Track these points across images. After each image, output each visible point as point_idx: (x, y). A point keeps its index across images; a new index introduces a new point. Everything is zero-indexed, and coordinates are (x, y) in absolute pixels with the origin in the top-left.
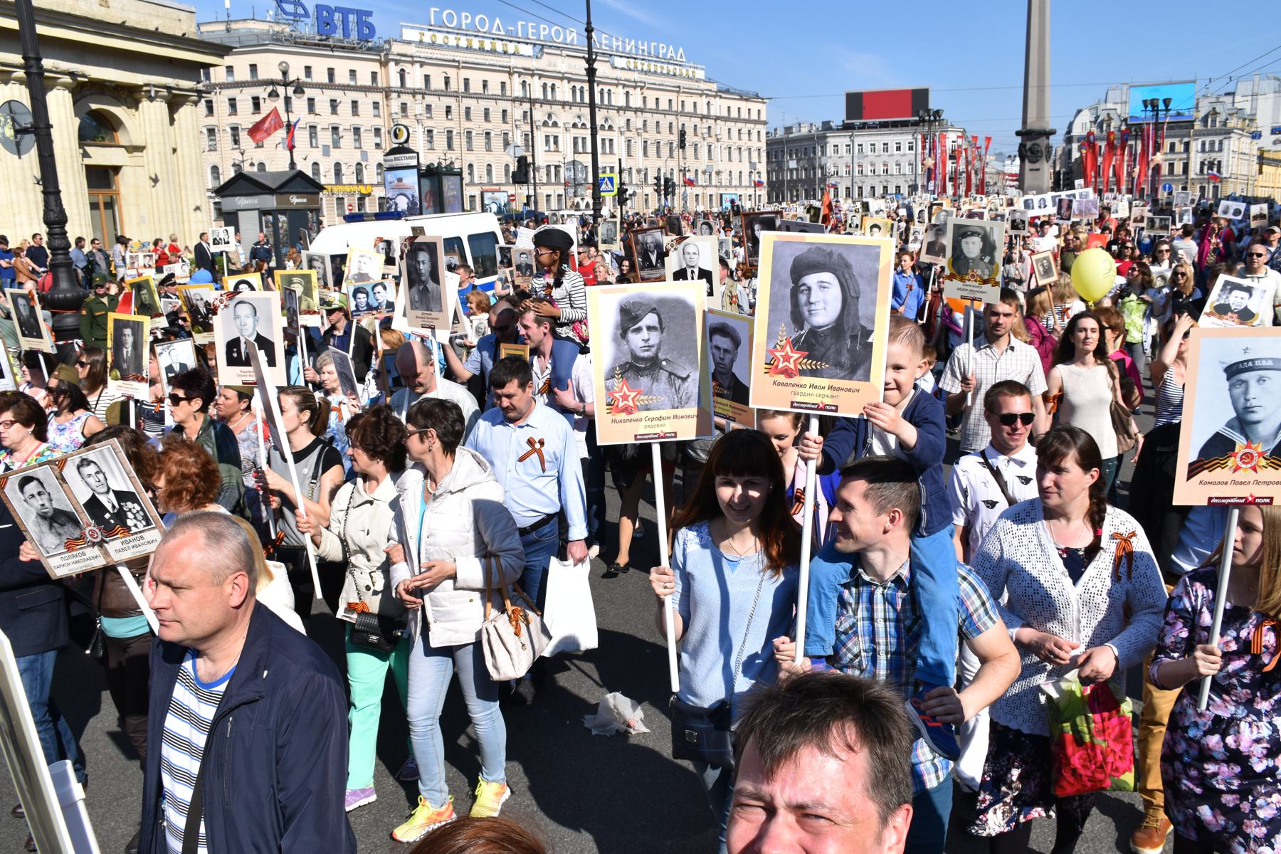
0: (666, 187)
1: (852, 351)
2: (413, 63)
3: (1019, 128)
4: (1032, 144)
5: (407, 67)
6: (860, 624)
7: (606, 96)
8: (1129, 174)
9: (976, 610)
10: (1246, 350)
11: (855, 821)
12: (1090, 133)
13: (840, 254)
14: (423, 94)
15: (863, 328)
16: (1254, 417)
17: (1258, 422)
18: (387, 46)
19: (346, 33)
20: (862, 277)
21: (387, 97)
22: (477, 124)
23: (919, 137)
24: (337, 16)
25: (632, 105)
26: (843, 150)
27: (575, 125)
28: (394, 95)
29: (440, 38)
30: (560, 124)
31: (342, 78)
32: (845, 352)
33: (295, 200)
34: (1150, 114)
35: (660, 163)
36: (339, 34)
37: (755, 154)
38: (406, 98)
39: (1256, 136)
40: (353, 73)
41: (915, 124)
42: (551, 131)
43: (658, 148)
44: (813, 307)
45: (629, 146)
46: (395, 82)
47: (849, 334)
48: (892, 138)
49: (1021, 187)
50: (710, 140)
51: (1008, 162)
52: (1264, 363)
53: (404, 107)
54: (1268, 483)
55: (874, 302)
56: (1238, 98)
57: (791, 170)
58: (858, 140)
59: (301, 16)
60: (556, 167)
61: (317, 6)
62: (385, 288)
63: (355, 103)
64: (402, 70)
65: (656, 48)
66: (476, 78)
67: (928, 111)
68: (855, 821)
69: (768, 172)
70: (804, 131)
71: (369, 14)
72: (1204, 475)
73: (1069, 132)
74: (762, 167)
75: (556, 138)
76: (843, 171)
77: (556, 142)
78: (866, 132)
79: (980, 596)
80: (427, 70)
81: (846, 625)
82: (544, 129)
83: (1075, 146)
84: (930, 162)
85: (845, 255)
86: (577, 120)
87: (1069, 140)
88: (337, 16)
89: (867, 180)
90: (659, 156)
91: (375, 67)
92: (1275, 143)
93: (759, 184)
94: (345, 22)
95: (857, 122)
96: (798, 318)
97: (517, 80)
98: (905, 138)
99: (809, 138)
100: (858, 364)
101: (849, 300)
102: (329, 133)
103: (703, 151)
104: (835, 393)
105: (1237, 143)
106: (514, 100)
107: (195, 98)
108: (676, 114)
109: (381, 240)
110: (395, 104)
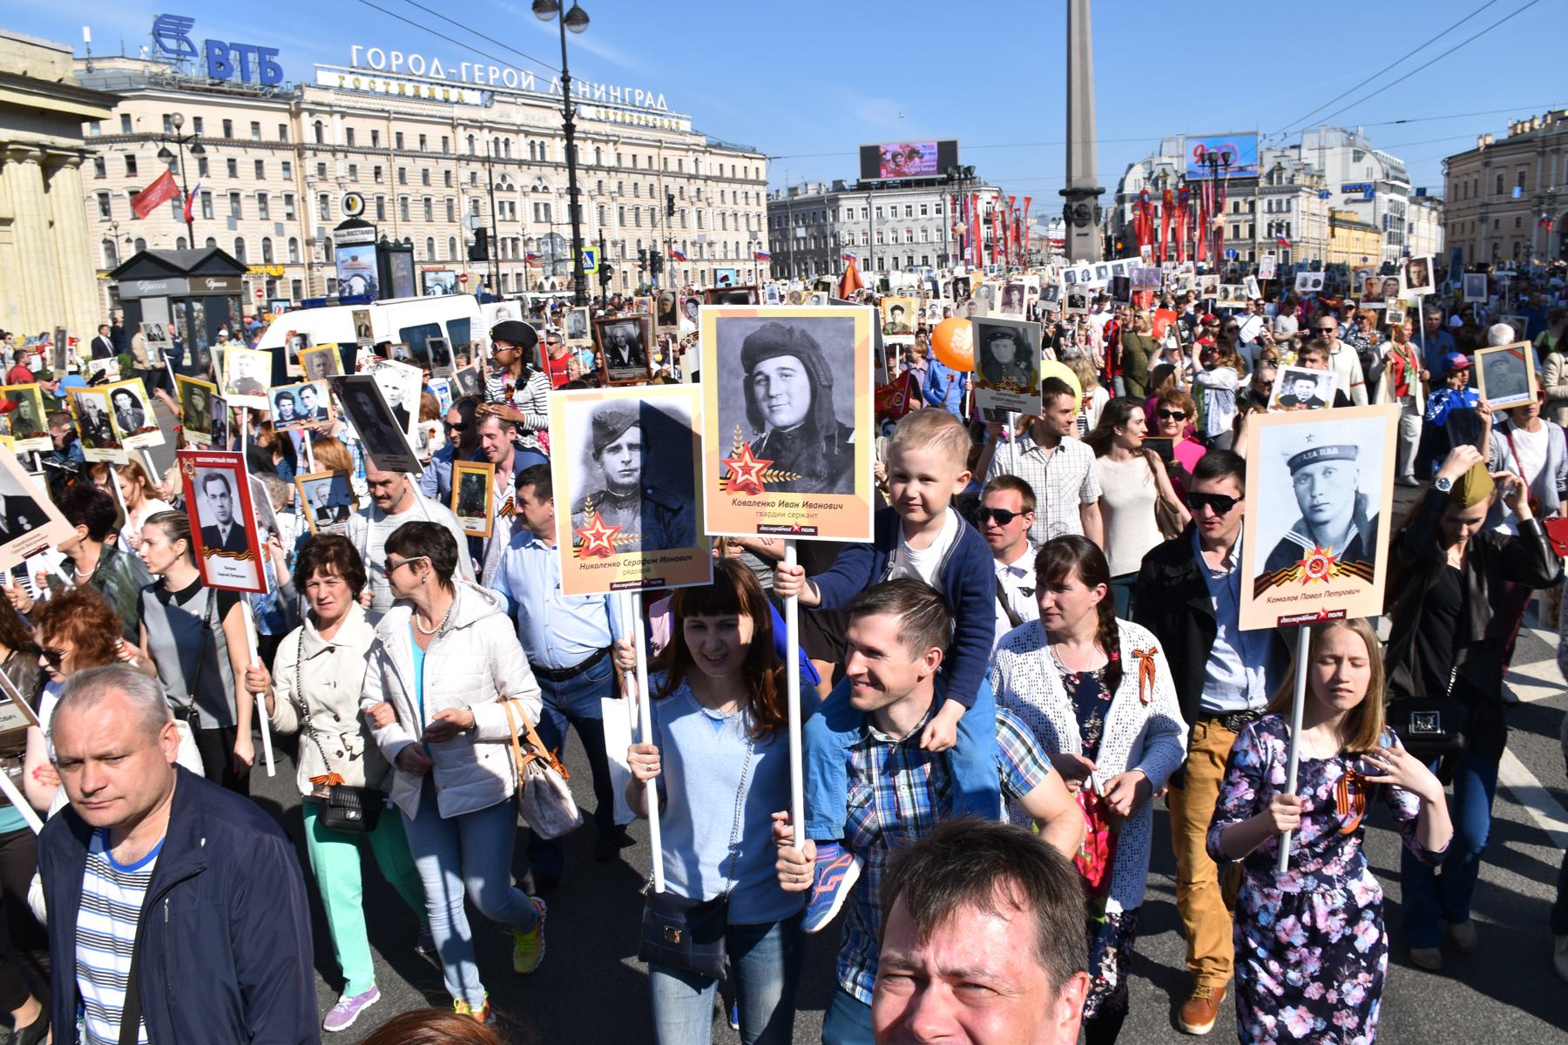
0: (653, 262)
1: (828, 456)
2: (331, 113)
3: (1063, 187)
4: (1078, 204)
5: (325, 119)
6: (877, 794)
7: (538, 149)
8: (1190, 239)
9: (1022, 760)
10: (1309, 438)
11: (1021, 991)
12: (1144, 192)
13: (803, 331)
14: (346, 152)
15: (841, 426)
16: (1321, 517)
17: (1326, 522)
18: (298, 93)
19: (246, 76)
20: (834, 359)
21: (300, 156)
22: (414, 189)
23: (948, 198)
24: (233, 55)
25: (604, 163)
26: (859, 214)
27: (535, 189)
28: (309, 154)
29: (365, 83)
30: (516, 187)
31: (241, 131)
32: (820, 457)
33: (212, 284)
34: (1207, 170)
35: (639, 234)
36: (236, 77)
37: (753, 222)
38: (324, 157)
39: (1324, 195)
40: (255, 125)
41: (943, 182)
42: (541, 198)
43: (637, 215)
44: (774, 402)
45: (601, 214)
46: (310, 137)
47: (823, 434)
48: (917, 199)
49: (1067, 255)
50: (699, 205)
51: (1052, 226)
52: (1330, 452)
53: (322, 168)
54: (1339, 594)
55: (851, 392)
56: (1305, 152)
57: (798, 240)
58: (876, 203)
59: (186, 53)
60: (514, 240)
61: (207, 42)
62: (315, 391)
63: (259, 164)
64: (318, 122)
65: (632, 94)
66: (411, 133)
67: (958, 168)
68: (1021, 991)
69: (770, 242)
70: (812, 193)
71: (275, 52)
72: (1272, 591)
73: (1121, 190)
74: (764, 236)
75: (512, 204)
76: (860, 240)
77: (512, 210)
78: (885, 192)
79: (1024, 742)
80: (350, 122)
81: (861, 798)
82: (533, 195)
83: (1128, 206)
84: (962, 227)
85: (809, 332)
86: (537, 183)
87: (1121, 199)
88: (233, 55)
89: (888, 250)
90: (638, 225)
91: (284, 118)
92: (1346, 202)
93: (759, 256)
94: (243, 62)
95: (874, 181)
96: (756, 417)
97: (462, 134)
98: (931, 199)
99: (818, 201)
100: (838, 474)
101: (819, 390)
102: (228, 200)
103: (692, 218)
104: (812, 511)
105: (1305, 203)
106: (460, 158)
107: (77, 159)
108: (658, 174)
109: (294, 334)
110: (311, 164)
